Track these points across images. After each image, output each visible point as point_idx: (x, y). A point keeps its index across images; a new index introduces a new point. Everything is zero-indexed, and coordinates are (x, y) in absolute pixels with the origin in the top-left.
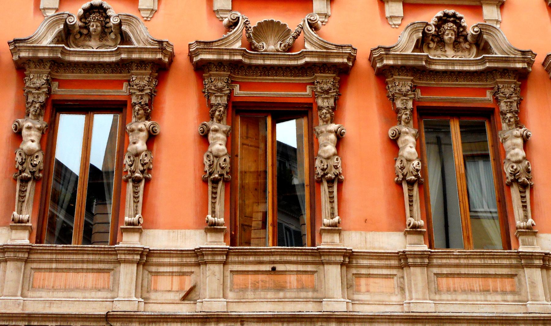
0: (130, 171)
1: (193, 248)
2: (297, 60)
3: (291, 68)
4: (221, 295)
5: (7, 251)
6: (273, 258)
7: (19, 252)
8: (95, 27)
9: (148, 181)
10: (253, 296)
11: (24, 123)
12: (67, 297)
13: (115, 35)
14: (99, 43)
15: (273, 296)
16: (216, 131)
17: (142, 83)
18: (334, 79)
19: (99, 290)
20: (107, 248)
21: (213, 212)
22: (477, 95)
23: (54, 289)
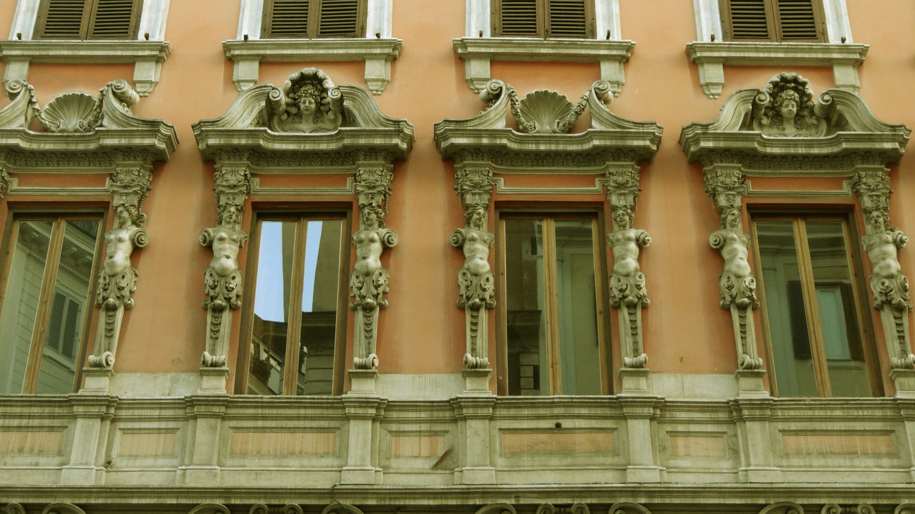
0: (359, 296)
8: (307, 104)
13: (335, 114)
14: (312, 126)
17: (371, 178)
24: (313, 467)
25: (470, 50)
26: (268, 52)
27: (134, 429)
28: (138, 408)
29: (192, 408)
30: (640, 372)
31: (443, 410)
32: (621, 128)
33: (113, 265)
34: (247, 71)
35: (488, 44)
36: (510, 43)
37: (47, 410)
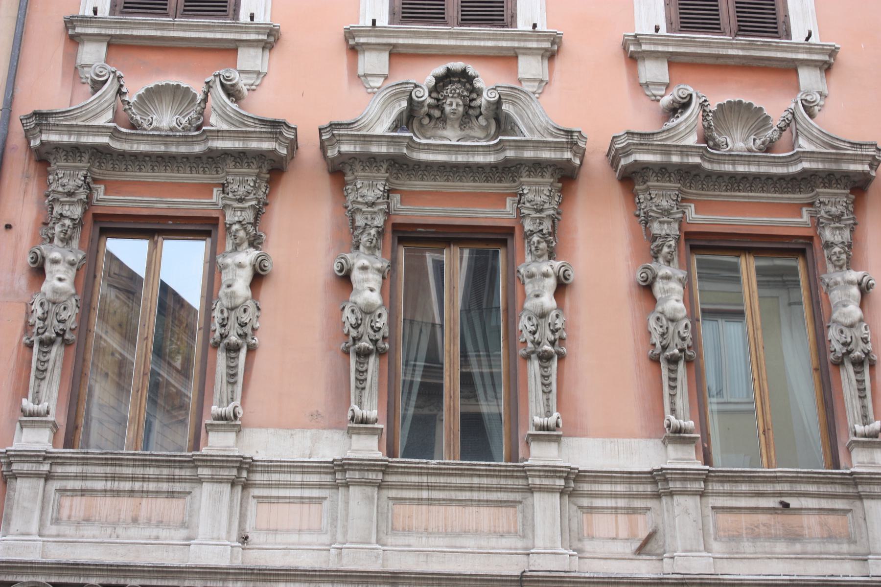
0: (533, 342)
1: (648, 469)
2: (787, 166)
3: (775, 179)
4: (702, 548)
5: (349, 469)
6: (779, 487)
7: (368, 470)
8: (454, 106)
9: (251, 350)
10: (752, 549)
11: (355, 261)
12: (452, 547)
13: (487, 119)
14: (459, 133)
15: (785, 550)
16: (667, 278)
17: (538, 199)
18: (551, 185)
19: (502, 536)
20: (510, 466)
21: (673, 411)
22: (772, 217)
23: (428, 532)
24: (494, 548)
25: (645, 47)
26: (401, 41)
27: (271, 497)
28: (275, 472)
29: (340, 472)
30: (874, 442)
31: (643, 483)
32: (834, 149)
33: (232, 296)
34: (374, 62)
35: (665, 42)
36: (692, 42)
37: (165, 471)
